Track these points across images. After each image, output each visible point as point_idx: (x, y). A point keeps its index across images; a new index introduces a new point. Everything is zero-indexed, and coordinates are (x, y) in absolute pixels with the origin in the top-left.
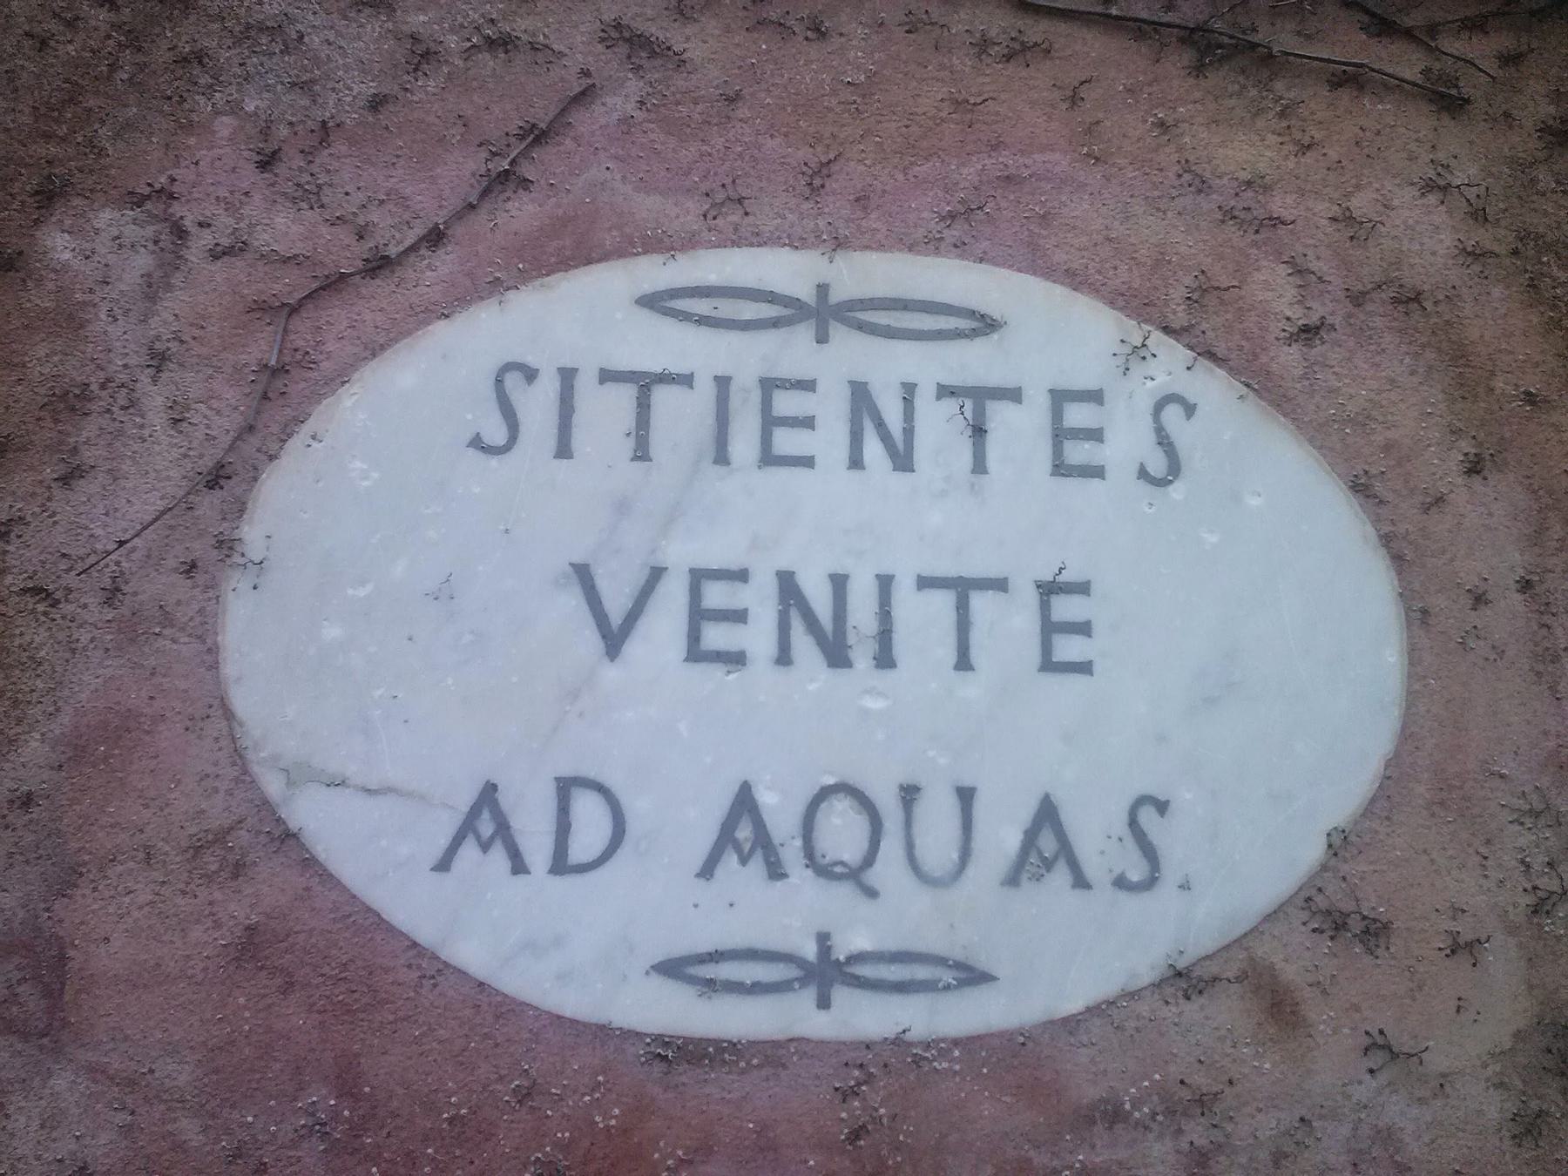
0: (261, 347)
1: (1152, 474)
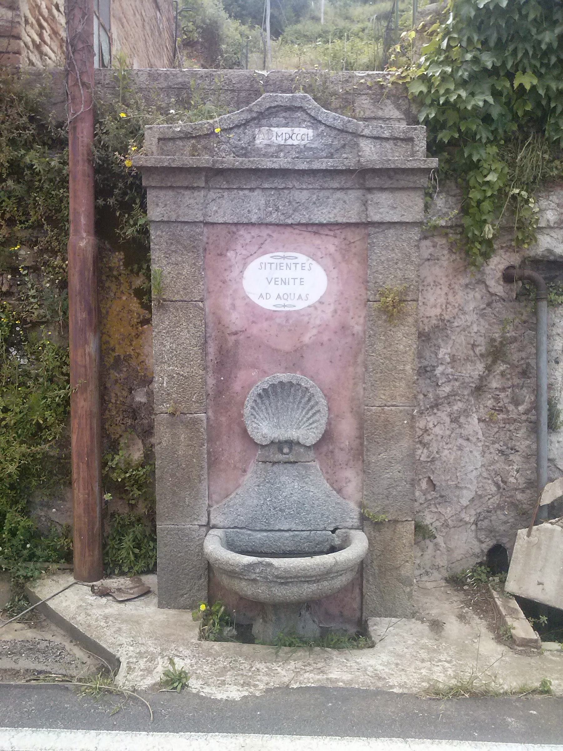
0: (243, 262)
1: (546, 525)
